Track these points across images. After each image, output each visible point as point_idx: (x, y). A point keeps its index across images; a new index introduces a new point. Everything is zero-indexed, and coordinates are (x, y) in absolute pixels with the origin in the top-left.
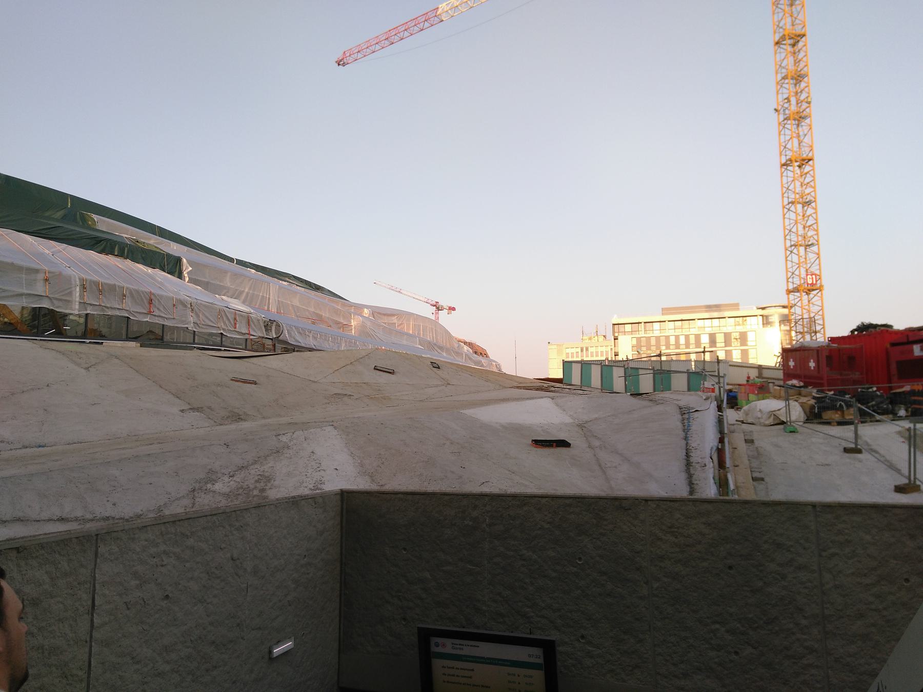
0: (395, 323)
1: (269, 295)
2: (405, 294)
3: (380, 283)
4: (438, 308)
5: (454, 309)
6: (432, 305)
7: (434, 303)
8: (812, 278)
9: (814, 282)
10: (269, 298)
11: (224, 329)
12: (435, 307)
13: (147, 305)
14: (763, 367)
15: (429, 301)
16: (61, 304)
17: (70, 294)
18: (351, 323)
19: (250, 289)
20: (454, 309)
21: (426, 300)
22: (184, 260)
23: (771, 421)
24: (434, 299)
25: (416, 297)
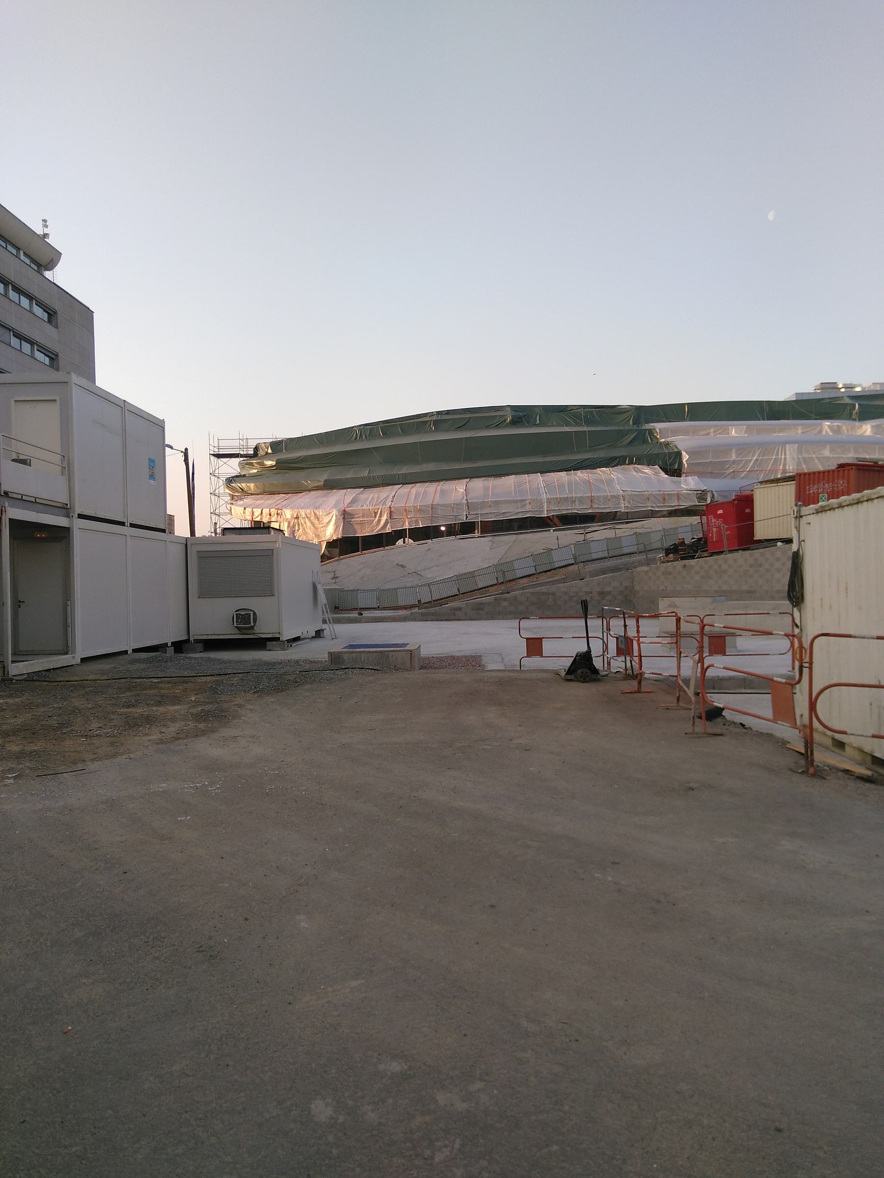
1: (785, 454)
10: (785, 458)
11: (651, 507)
19: (759, 456)
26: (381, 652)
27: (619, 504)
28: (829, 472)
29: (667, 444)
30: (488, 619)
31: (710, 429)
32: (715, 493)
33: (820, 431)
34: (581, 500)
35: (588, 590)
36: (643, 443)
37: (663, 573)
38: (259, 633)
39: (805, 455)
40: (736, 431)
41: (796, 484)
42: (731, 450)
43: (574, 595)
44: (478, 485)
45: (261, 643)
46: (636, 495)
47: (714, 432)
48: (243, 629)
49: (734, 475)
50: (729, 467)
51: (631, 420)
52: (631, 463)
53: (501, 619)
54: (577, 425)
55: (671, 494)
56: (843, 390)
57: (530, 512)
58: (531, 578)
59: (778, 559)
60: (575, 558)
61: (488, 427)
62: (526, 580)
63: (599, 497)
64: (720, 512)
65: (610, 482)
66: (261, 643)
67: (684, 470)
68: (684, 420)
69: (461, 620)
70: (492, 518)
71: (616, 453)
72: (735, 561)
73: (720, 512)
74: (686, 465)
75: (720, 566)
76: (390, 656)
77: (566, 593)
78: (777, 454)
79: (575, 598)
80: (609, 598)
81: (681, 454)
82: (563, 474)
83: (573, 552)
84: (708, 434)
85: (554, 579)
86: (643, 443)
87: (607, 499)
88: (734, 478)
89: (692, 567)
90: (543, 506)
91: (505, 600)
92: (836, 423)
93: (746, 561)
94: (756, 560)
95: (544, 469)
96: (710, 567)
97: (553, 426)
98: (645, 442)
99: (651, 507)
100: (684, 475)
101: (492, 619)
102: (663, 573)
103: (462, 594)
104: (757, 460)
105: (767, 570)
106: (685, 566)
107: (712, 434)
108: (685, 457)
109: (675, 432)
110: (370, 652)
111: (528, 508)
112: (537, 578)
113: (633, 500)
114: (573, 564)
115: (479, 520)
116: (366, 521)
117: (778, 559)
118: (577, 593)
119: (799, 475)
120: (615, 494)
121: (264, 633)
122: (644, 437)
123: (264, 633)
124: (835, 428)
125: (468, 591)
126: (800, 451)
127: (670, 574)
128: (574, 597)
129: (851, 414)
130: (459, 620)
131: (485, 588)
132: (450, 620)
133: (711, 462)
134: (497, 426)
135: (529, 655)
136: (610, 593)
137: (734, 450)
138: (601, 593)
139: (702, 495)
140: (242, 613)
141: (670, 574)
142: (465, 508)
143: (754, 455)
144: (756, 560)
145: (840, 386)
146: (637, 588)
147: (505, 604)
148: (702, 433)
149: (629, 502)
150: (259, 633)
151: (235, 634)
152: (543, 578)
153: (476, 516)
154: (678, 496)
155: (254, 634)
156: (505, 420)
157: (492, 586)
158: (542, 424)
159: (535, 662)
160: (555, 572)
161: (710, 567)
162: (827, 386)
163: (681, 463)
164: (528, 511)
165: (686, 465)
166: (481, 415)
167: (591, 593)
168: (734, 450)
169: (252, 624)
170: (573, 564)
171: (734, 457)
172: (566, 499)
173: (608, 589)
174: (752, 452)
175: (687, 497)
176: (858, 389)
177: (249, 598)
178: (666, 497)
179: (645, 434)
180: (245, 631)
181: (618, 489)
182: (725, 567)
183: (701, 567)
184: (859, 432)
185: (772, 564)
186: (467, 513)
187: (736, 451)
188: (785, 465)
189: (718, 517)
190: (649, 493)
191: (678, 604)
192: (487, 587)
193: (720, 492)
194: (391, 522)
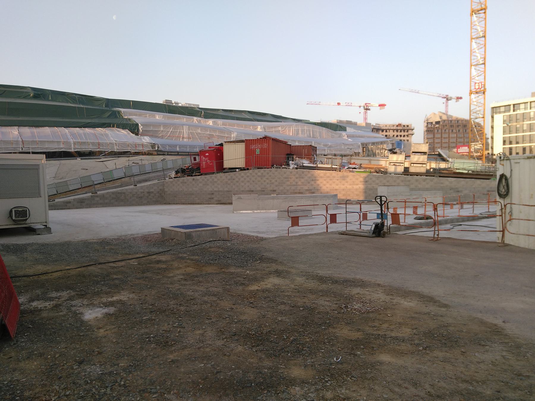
0: (280, 130)
1: (183, 130)
2: (422, 94)
3: (403, 89)
4: (448, 99)
5: (461, 98)
6: (443, 98)
7: (445, 96)
8: (479, 85)
9: (480, 87)
10: (183, 132)
11: (130, 150)
12: (445, 99)
13: (98, 146)
14: (86, 153)
15: (441, 95)
16: (68, 149)
17: (71, 146)
18: (231, 135)
19: (172, 129)
20: (461, 98)
21: (438, 95)
22: (140, 125)
23: (526, 158)
24: (445, 94)
25: (431, 94)
26: (213, 230)
27: (113, 147)
28: (254, 140)
29: (130, 119)
30: (87, 208)
31: (147, 115)
32: (160, 146)
33: (193, 121)
34: (93, 144)
35: (142, 191)
36: (115, 117)
37: (182, 183)
38: (29, 223)
39: (191, 131)
40: (158, 117)
41: (245, 144)
42: (160, 126)
43: (134, 193)
44: (27, 131)
45: (30, 231)
46: (122, 143)
47: (149, 116)
48: (18, 221)
49: (162, 137)
50: (160, 133)
51: (104, 105)
52: (113, 127)
53: (95, 207)
54: (74, 103)
55: (139, 144)
56: (174, 104)
57: (63, 149)
58: (101, 185)
59: (242, 177)
60: (125, 175)
61: (19, 97)
62: (99, 186)
63: (103, 143)
64: (207, 154)
65: (107, 135)
66: (30, 231)
67: (140, 133)
68: (131, 109)
69: (71, 209)
70: (39, 150)
71: (103, 121)
72: (221, 177)
73: (207, 154)
74: (141, 131)
75: (213, 180)
76: (218, 231)
77: (131, 193)
78: (180, 130)
79: (136, 195)
80: (152, 195)
81: (138, 125)
82: (78, 129)
83: (124, 171)
84: (146, 117)
85: (115, 185)
86: (115, 117)
87: (107, 144)
88: (162, 138)
89: (198, 180)
90: (71, 146)
91: (97, 196)
92: (199, 119)
93: (226, 177)
94: (232, 177)
95: (20, 124)
96: (208, 180)
97: (59, 102)
98: (116, 117)
99: (130, 150)
100: (140, 135)
101: (90, 207)
102: (182, 183)
103: (59, 194)
104: (172, 131)
105: (237, 182)
106: (194, 179)
107: (148, 117)
108: (141, 128)
109: (131, 114)
110: (207, 230)
111: (62, 146)
112: (105, 185)
113: (121, 146)
114: (124, 177)
115: (31, 151)
116: (280, 128)
117: (242, 177)
118: (136, 193)
119: (247, 140)
120: (112, 142)
121: (34, 223)
122: (116, 115)
123: (34, 223)
124: (199, 120)
125: (63, 192)
126: (189, 130)
127: (186, 183)
128: (135, 194)
129: (201, 115)
130: (69, 209)
131: (74, 190)
132: (64, 209)
133: (152, 130)
134: (25, 97)
135: (293, 225)
136: (152, 192)
137: (162, 126)
138: (149, 193)
139: (153, 145)
140: (19, 210)
141: (186, 183)
142: (21, 143)
143: (171, 129)
144: (232, 177)
145: (173, 102)
146: (166, 190)
147: (98, 199)
148: (143, 116)
149: (119, 147)
150: (29, 223)
151: (10, 225)
152: (109, 185)
153: (28, 149)
154: (143, 145)
155: (26, 224)
156: (30, 95)
157: (78, 189)
158: (52, 100)
159: (333, 228)
160: (115, 181)
161: (208, 180)
162: (168, 101)
163: (138, 129)
164: (62, 148)
165: (141, 131)
166: (10, 90)
167: (144, 192)
168: (162, 126)
169: (28, 216)
170: (124, 177)
171: (162, 129)
172: (85, 143)
173: (152, 190)
174: (170, 128)
175: (147, 146)
176: (180, 105)
177: (16, 199)
178: (137, 145)
179: (116, 113)
180: (19, 223)
181: (112, 140)
182: (215, 180)
183: (203, 180)
184: (208, 123)
185: (239, 179)
186: (23, 147)
187: (163, 126)
188: (183, 135)
189: (206, 157)
190: (129, 143)
191: (242, 197)
192: (75, 190)
193: (162, 145)
194: (428, 155)
